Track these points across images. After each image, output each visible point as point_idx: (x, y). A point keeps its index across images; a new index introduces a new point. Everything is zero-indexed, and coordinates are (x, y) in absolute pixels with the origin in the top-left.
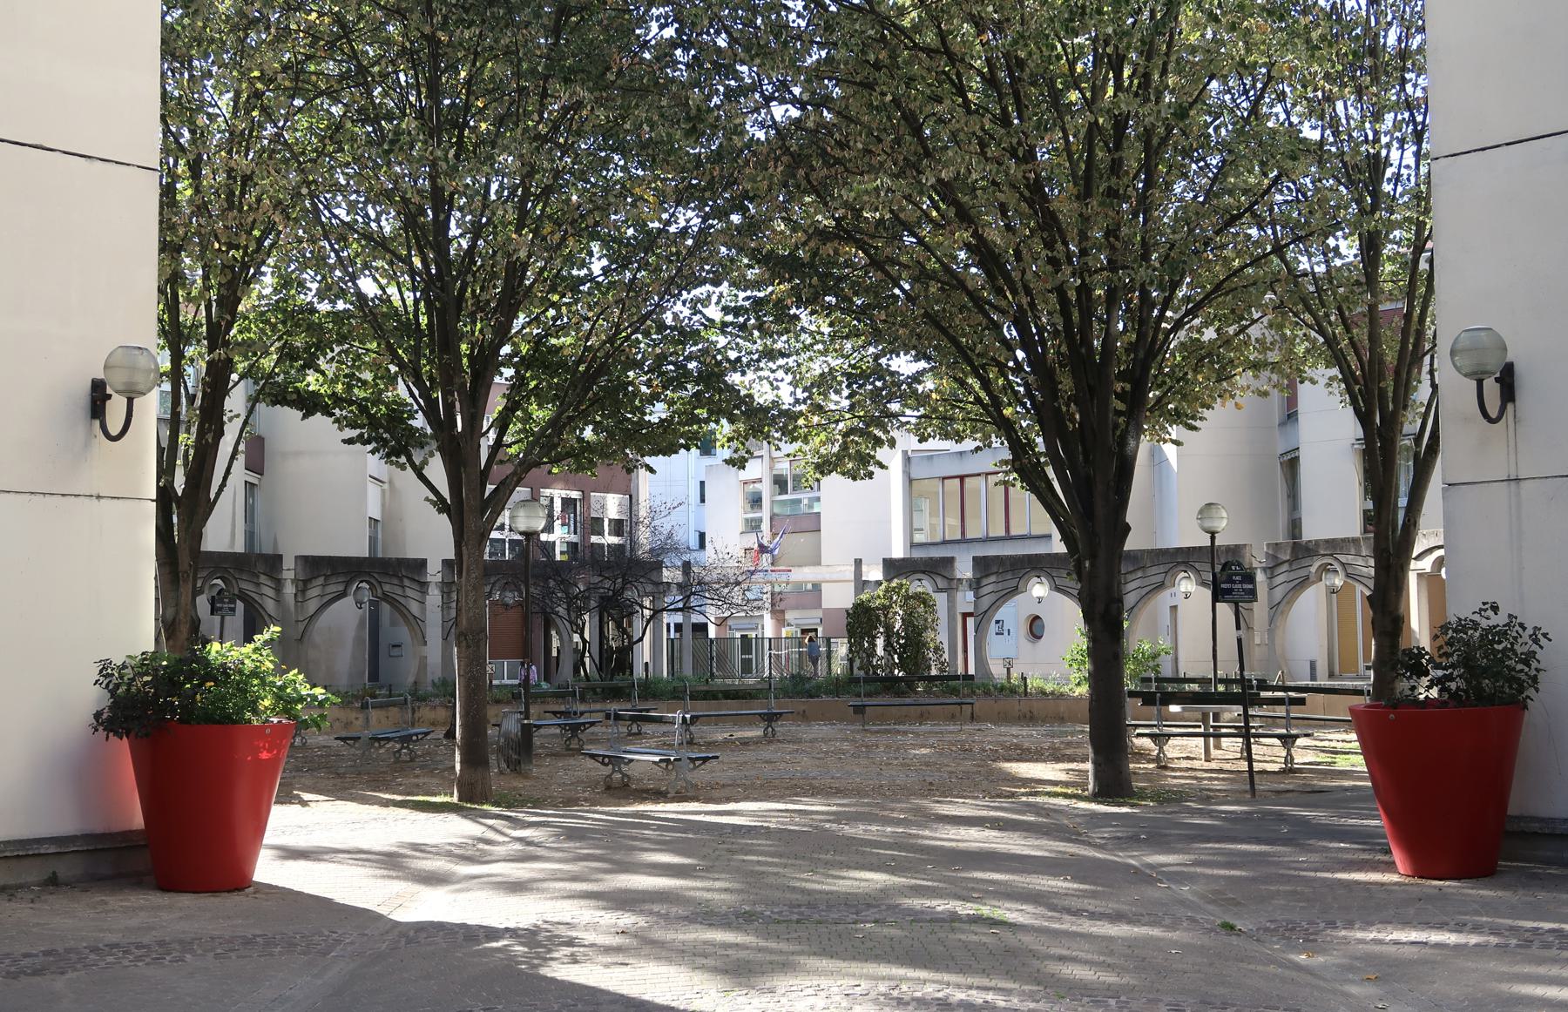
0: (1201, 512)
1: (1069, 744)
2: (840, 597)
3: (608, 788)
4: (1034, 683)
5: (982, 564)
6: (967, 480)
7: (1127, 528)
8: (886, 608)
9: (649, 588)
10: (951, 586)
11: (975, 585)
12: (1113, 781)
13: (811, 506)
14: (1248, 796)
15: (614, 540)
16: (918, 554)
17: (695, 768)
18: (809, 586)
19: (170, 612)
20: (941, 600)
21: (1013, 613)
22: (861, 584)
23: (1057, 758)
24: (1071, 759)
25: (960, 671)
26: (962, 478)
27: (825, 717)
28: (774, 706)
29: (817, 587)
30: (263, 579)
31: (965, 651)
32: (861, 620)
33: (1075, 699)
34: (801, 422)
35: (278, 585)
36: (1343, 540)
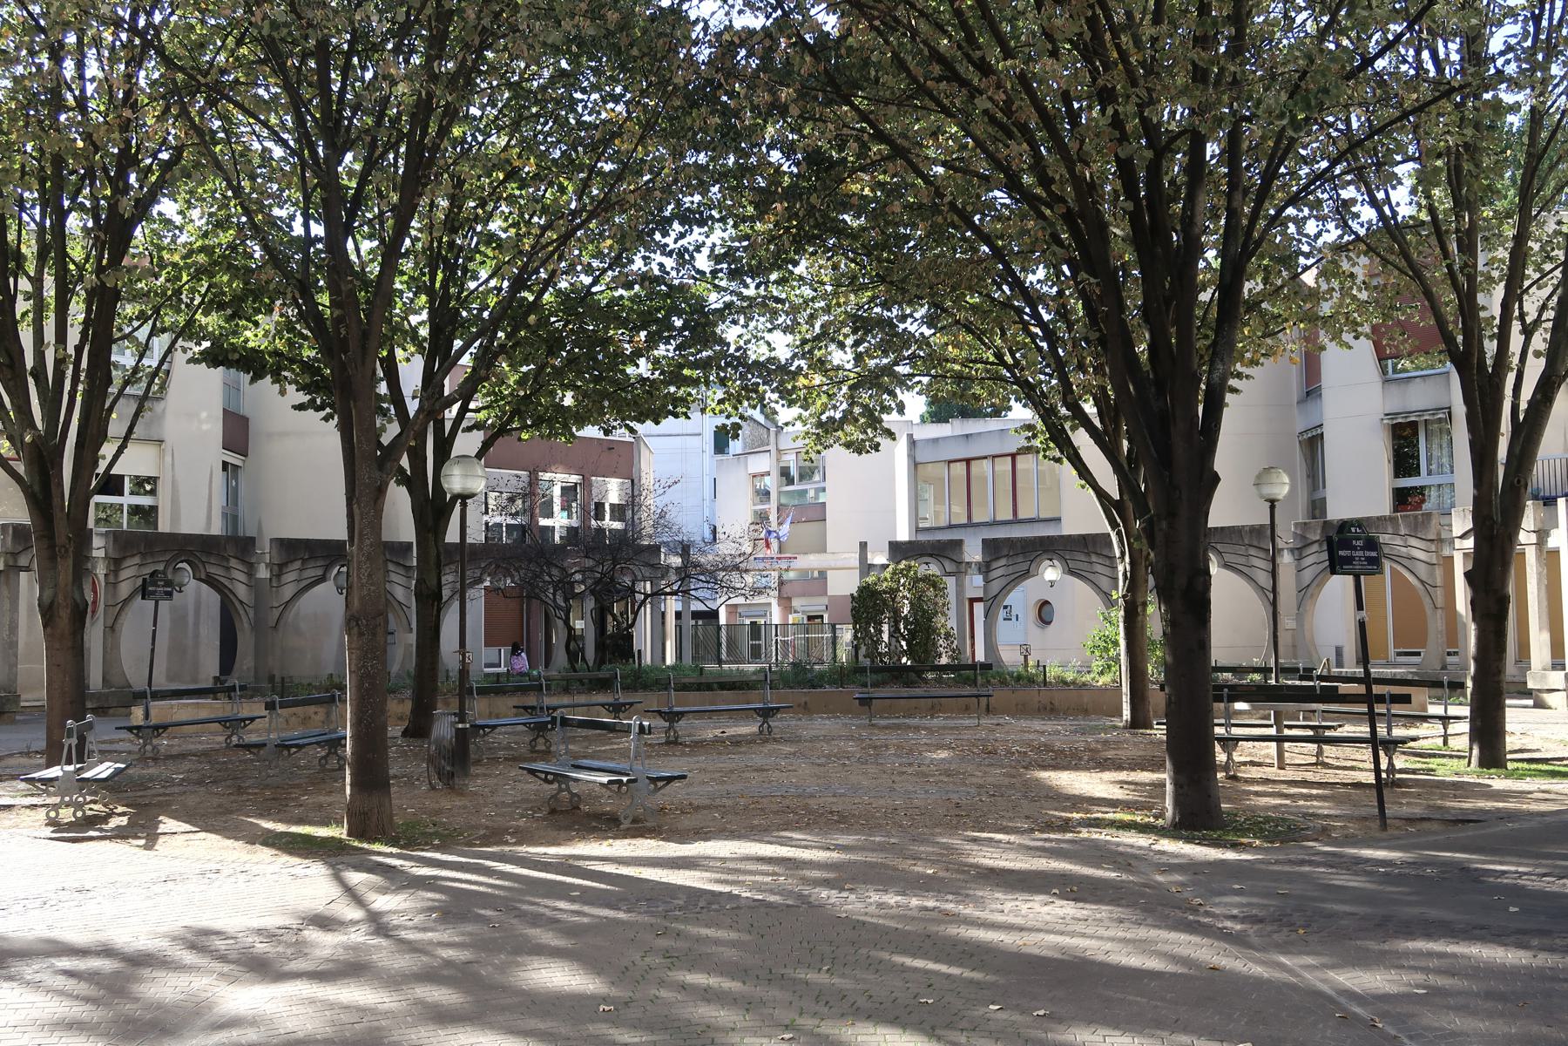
0: (1259, 477)
1: (1106, 742)
2: (845, 584)
3: (553, 812)
4: (1053, 672)
5: (991, 547)
6: (974, 465)
7: (1215, 479)
8: (893, 592)
9: (647, 572)
10: (960, 569)
11: (985, 568)
12: (1199, 813)
13: (817, 497)
14: (1376, 825)
15: (617, 525)
16: (922, 538)
17: (658, 789)
18: (816, 574)
19: (48, 593)
20: (950, 582)
21: (1022, 598)
22: (866, 568)
23: (1103, 765)
24: (1119, 767)
25: (980, 656)
26: (968, 461)
27: (829, 710)
28: (771, 698)
29: (823, 574)
30: (233, 563)
31: (973, 637)
32: (868, 605)
33: (1100, 689)
34: (802, 381)
35: (251, 570)
36: (1379, 518)
